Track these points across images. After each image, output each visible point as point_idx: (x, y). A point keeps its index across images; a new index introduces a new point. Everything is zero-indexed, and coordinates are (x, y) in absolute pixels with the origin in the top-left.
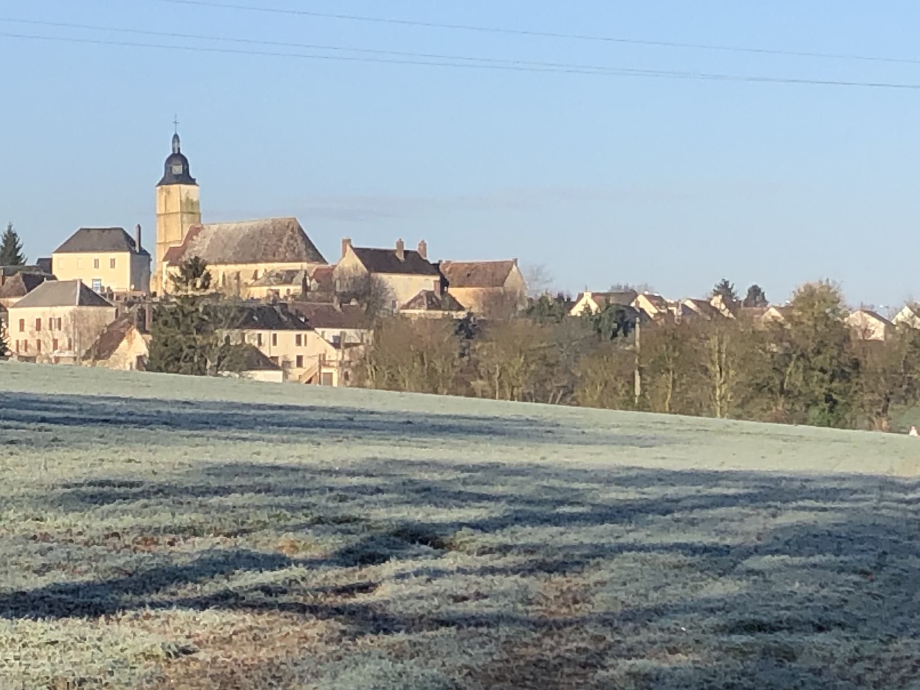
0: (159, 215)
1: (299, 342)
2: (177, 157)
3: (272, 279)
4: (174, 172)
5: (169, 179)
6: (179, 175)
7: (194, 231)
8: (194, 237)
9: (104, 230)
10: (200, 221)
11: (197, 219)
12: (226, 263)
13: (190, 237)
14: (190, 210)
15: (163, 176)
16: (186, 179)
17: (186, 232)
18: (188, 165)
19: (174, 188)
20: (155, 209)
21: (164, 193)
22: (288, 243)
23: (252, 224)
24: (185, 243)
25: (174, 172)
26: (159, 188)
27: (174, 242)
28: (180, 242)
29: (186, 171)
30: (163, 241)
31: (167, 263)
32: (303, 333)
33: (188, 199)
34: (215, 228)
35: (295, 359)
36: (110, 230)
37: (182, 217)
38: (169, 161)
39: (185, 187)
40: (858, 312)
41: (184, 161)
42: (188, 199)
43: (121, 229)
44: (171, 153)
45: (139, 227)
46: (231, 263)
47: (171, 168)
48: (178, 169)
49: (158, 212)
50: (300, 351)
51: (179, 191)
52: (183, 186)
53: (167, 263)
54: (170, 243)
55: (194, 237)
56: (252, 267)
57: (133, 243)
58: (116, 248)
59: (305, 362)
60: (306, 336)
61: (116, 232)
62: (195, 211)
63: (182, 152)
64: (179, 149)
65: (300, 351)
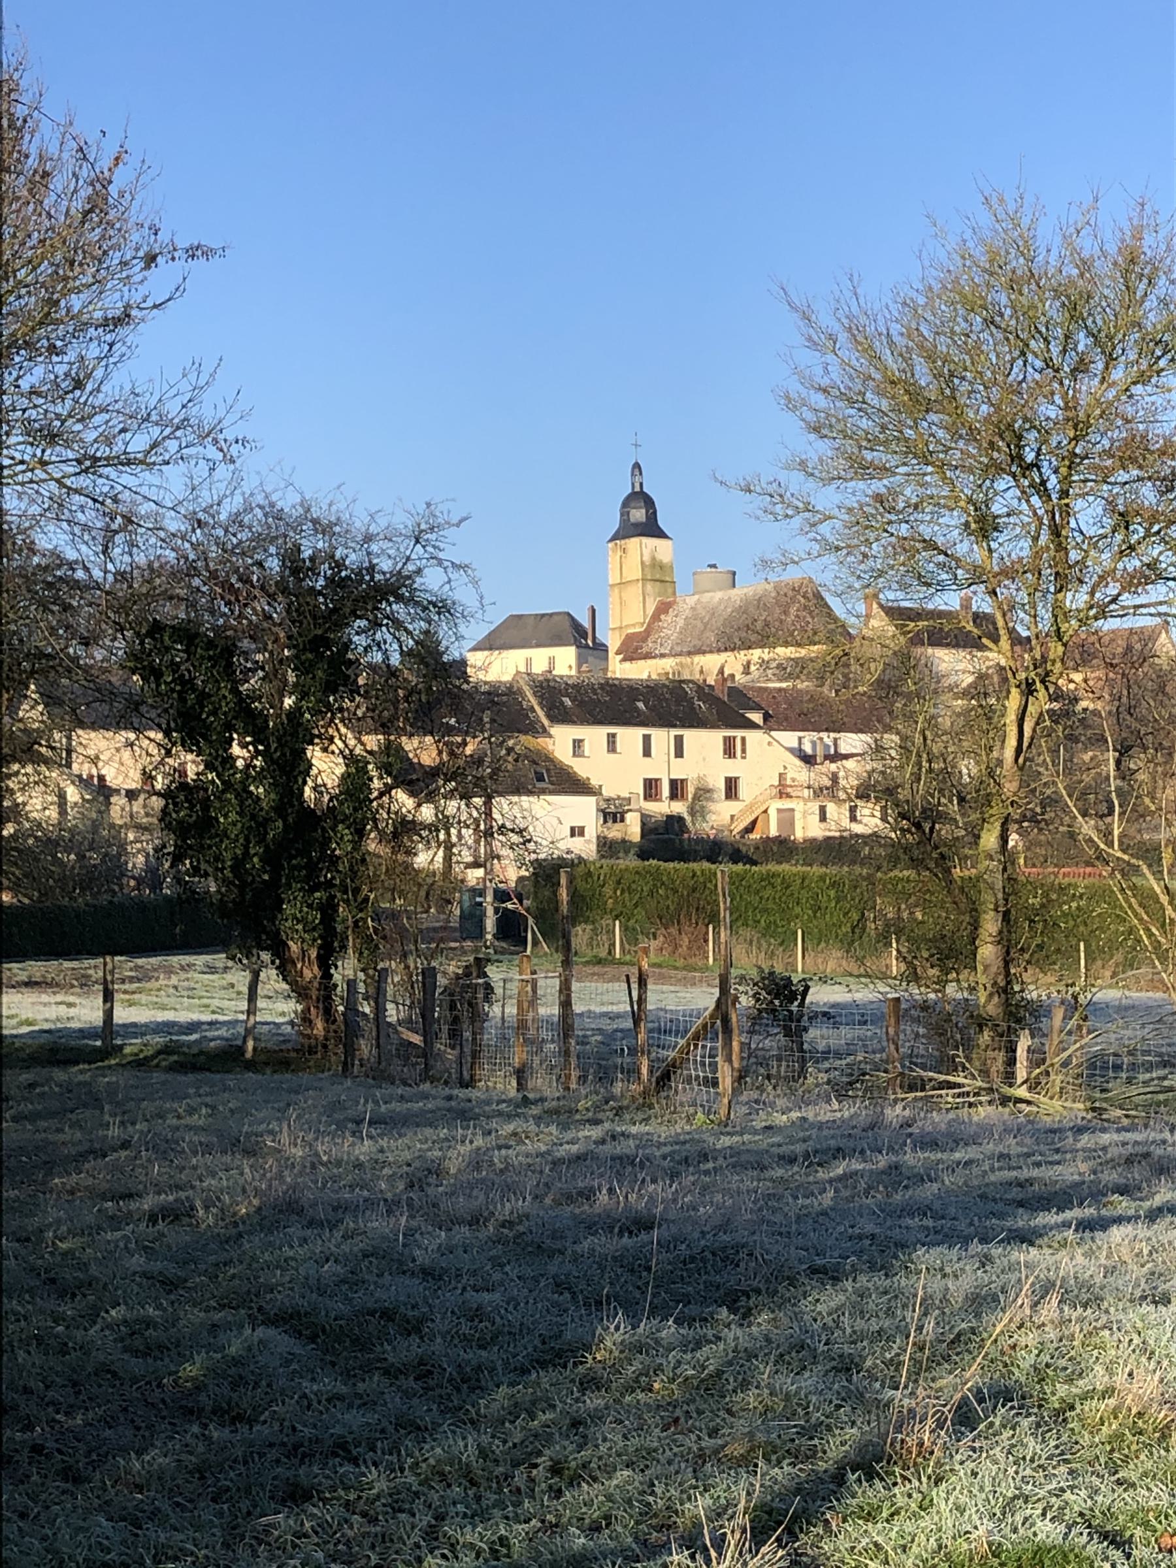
0: (612, 586)
1: (729, 750)
2: (640, 497)
3: (769, 672)
4: (632, 520)
5: (627, 530)
6: (642, 524)
7: (663, 608)
8: (663, 617)
9: (543, 615)
10: (674, 593)
11: (670, 591)
12: (704, 653)
13: (656, 617)
14: (658, 576)
15: (617, 526)
16: (651, 529)
17: (650, 612)
18: (655, 513)
19: (634, 543)
20: (607, 580)
21: (619, 553)
22: (797, 616)
23: (745, 590)
24: (649, 625)
25: (632, 520)
26: (610, 545)
27: (634, 625)
28: (642, 624)
29: (652, 516)
30: (618, 625)
31: (621, 656)
32: (738, 733)
33: (653, 558)
34: (692, 601)
35: (722, 785)
36: (551, 615)
37: (643, 586)
38: (626, 503)
39: (650, 542)
40: (564, 1520)
41: (649, 503)
42: (653, 558)
43: (569, 614)
44: (630, 491)
45: (594, 611)
46: (711, 652)
47: (628, 513)
48: (638, 515)
49: (611, 582)
50: (732, 768)
51: (641, 547)
52: (645, 540)
53: (621, 656)
54: (627, 626)
55: (663, 617)
56: (743, 656)
57: (584, 634)
58: (556, 640)
59: (743, 790)
60: (743, 739)
61: (560, 617)
62: (668, 579)
63: (645, 490)
64: (641, 484)
65: (732, 768)
